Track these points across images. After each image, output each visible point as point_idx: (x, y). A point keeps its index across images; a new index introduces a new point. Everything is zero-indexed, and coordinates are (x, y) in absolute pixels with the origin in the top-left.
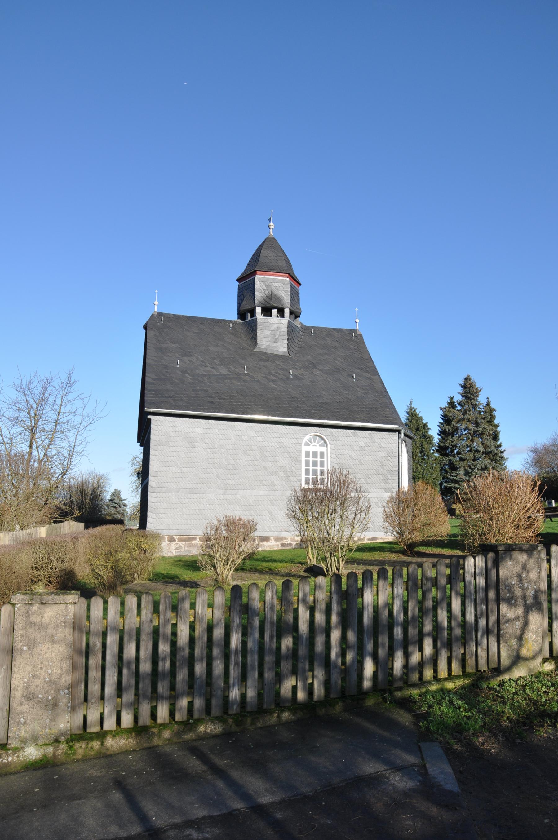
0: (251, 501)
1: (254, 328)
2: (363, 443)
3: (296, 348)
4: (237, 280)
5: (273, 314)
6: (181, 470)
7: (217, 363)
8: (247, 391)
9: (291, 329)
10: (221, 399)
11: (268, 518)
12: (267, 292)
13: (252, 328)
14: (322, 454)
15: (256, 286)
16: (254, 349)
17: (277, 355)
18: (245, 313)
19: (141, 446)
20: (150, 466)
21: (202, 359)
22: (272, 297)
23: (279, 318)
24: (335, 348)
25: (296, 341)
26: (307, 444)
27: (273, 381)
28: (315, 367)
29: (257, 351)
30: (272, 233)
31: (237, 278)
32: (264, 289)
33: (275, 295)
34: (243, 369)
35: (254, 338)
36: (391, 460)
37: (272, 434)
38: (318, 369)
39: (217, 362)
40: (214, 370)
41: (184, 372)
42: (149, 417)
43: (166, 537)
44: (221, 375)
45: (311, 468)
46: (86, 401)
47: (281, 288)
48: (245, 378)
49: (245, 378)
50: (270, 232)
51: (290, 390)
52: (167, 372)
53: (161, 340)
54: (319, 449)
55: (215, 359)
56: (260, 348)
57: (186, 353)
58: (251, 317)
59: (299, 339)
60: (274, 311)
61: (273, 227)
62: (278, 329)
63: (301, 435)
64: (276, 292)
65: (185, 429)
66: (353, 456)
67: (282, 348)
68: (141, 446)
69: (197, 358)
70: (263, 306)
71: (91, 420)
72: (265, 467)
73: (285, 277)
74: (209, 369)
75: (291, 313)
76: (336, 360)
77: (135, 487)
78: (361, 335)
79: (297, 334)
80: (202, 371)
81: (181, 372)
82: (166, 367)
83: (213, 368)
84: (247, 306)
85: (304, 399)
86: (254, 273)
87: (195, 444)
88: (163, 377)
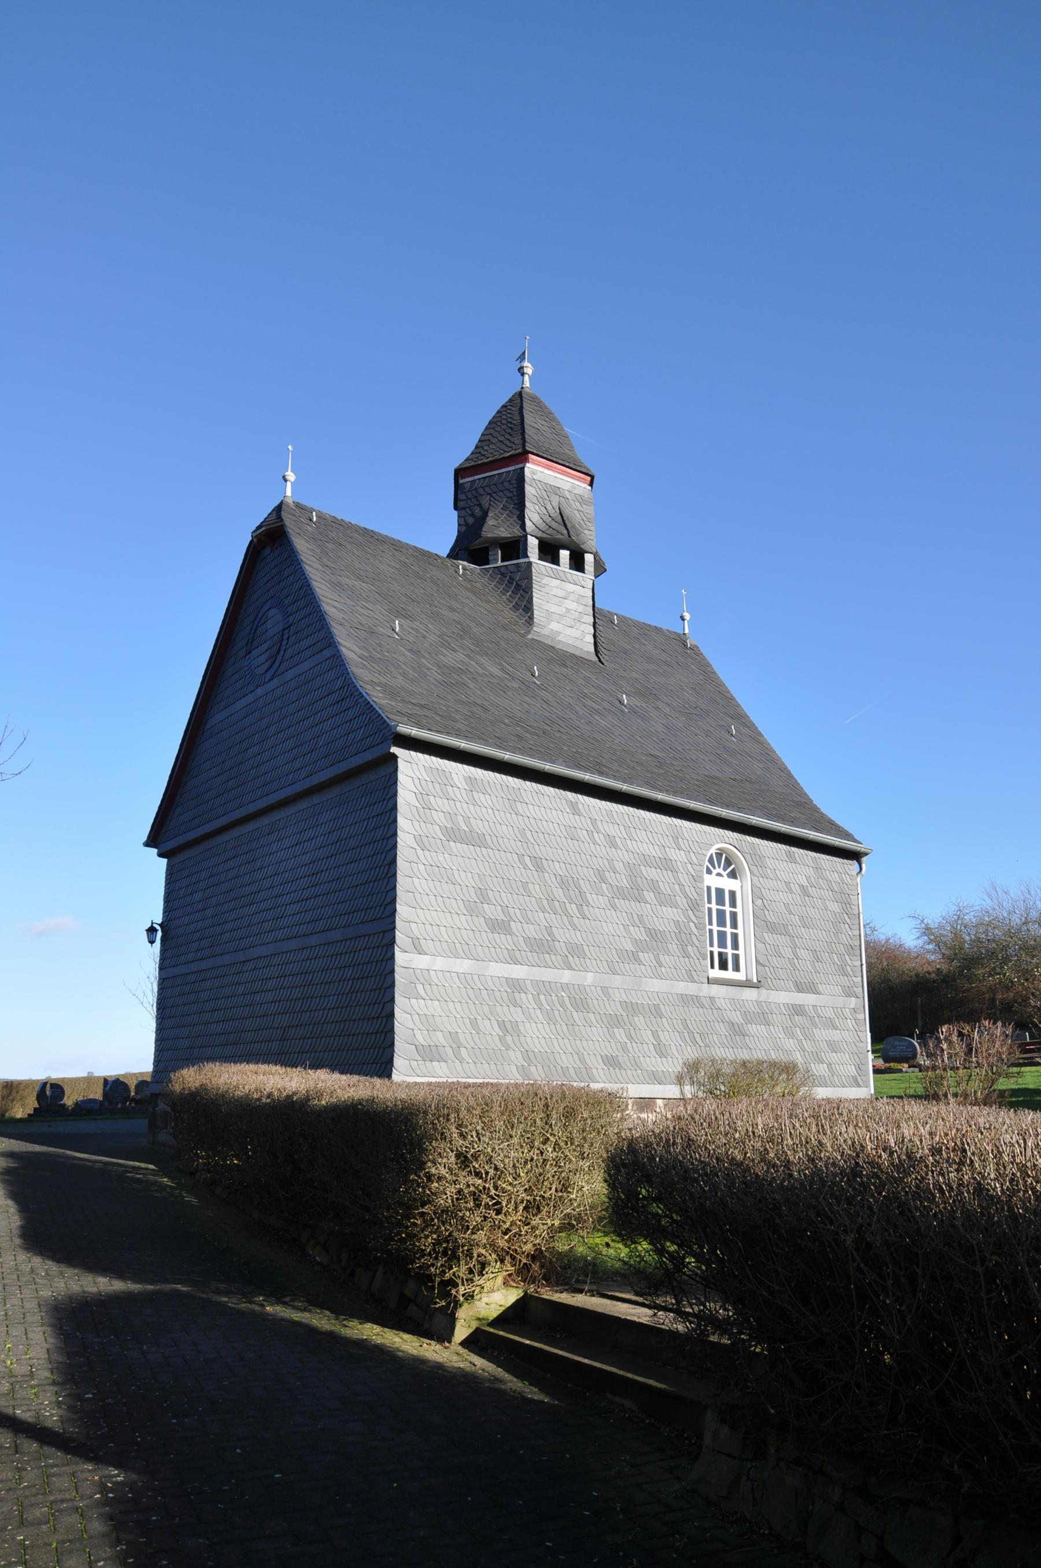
1: (524, 583)
5: (561, 561)
13: (519, 590)
14: (733, 894)
16: (529, 632)
19: (160, 855)
31: (456, 465)
35: (525, 607)
36: (848, 921)
42: (394, 750)
43: (630, 1102)
54: (728, 884)
60: (564, 554)
70: (545, 535)
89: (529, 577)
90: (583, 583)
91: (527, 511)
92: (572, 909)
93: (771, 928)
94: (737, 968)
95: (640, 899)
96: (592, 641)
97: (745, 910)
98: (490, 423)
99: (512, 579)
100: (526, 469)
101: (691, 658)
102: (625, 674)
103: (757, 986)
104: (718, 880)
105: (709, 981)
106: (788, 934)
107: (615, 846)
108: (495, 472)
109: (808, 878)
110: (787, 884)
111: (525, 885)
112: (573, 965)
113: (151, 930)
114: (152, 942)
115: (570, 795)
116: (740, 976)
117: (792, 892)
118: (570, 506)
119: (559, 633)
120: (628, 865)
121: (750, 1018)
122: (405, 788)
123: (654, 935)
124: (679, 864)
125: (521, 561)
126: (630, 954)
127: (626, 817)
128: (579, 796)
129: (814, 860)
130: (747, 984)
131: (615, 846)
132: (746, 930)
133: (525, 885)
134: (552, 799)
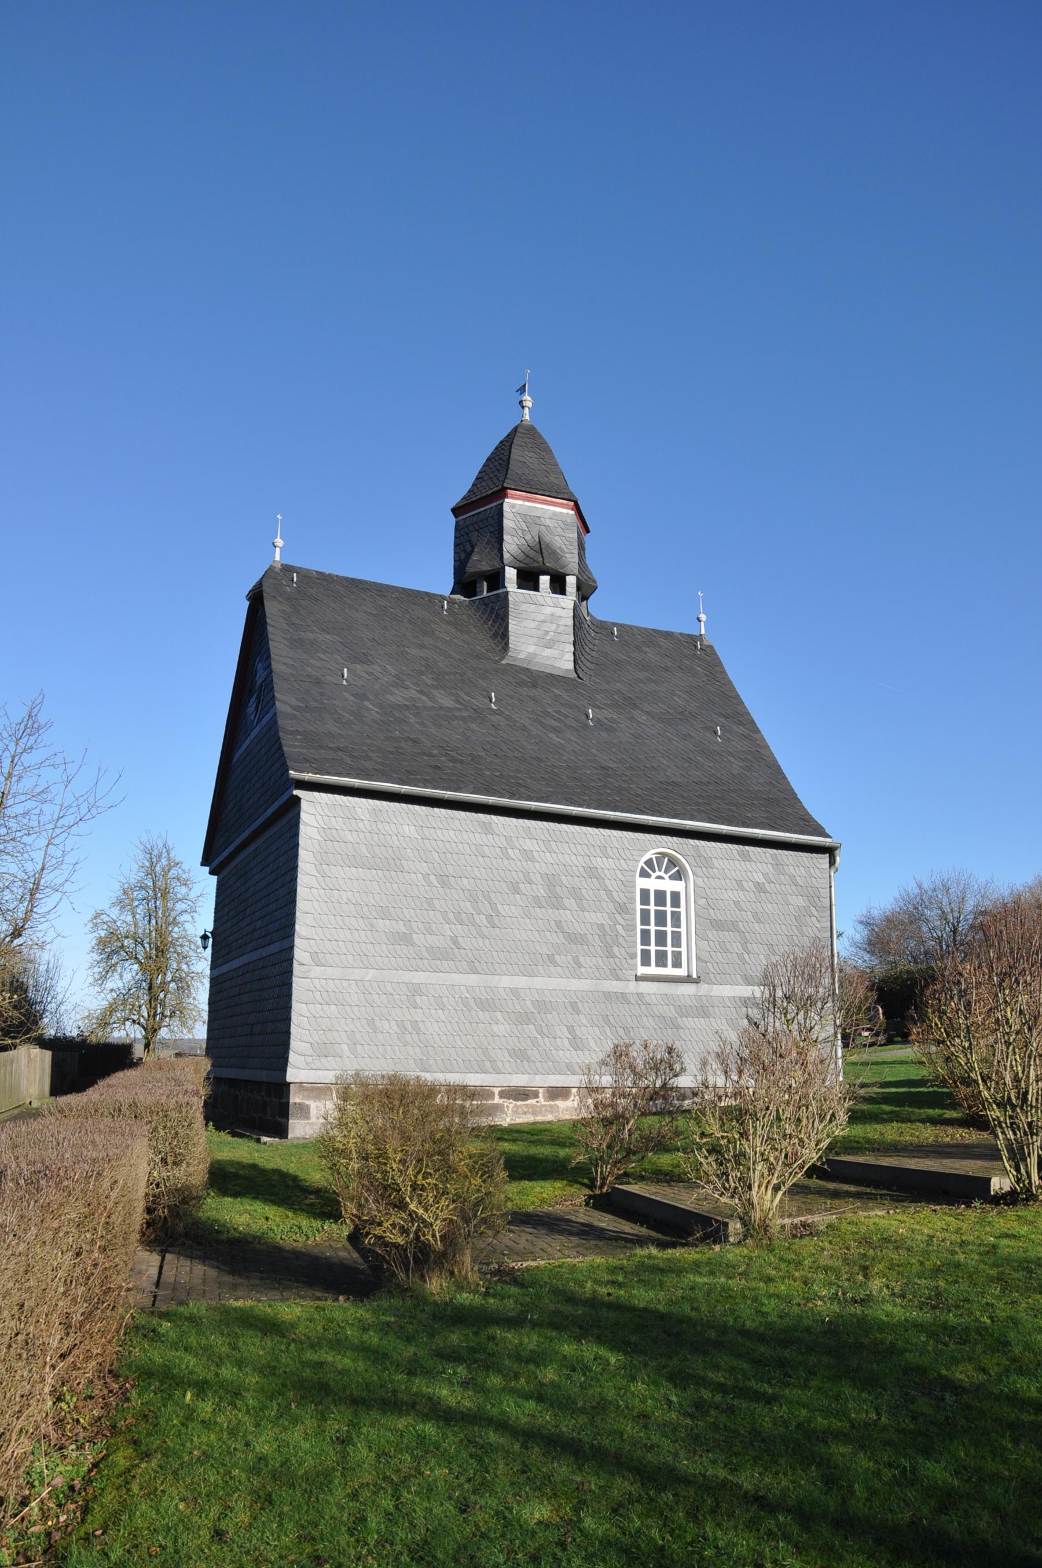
0: (528, 1003)
1: (501, 612)
2: (760, 875)
3: (588, 664)
5: (541, 586)
6: (372, 925)
7: (430, 682)
8: (504, 748)
10: (454, 761)
11: (566, 1043)
13: (497, 616)
14: (676, 896)
15: (506, 522)
16: (503, 658)
19: (211, 873)
20: (298, 914)
21: (394, 672)
22: (540, 547)
24: (666, 669)
25: (587, 649)
26: (644, 874)
27: (555, 730)
28: (635, 707)
31: (453, 505)
33: (548, 545)
34: (487, 701)
35: (502, 635)
36: (815, 913)
37: (572, 846)
38: (642, 711)
39: (427, 679)
40: (424, 698)
41: (362, 697)
42: (296, 792)
43: (541, 1090)
44: (441, 708)
45: (653, 928)
46: (71, 769)
48: (495, 719)
49: (495, 719)
51: (593, 751)
52: (322, 694)
53: (299, 622)
54: (670, 886)
55: (422, 673)
56: (515, 659)
57: (357, 658)
59: (591, 646)
60: (545, 580)
63: (634, 853)
64: (547, 538)
65: (380, 826)
66: (742, 904)
67: (561, 658)
68: (211, 873)
69: (384, 669)
70: (522, 565)
71: (84, 809)
72: (558, 923)
74: (412, 693)
76: (675, 694)
77: (97, 976)
78: (711, 647)
80: (398, 697)
81: (353, 695)
82: (318, 682)
83: (421, 692)
84: (480, 562)
85: (628, 773)
86: (501, 494)
87: (404, 863)
88: (315, 704)
89: (506, 606)
90: (563, 605)
91: (505, 544)
92: (481, 920)
93: (718, 925)
94: (677, 964)
95: (559, 906)
96: (572, 658)
97: (687, 910)
98: (488, 460)
99: (493, 609)
100: (505, 506)
101: (699, 659)
102: (607, 687)
103: (697, 981)
104: (661, 883)
105: (638, 979)
106: (737, 930)
107: (532, 860)
108: (482, 509)
109: (765, 876)
110: (739, 883)
111: (430, 901)
112: (480, 970)
113: (205, 937)
114: (205, 948)
115: (481, 816)
116: (682, 972)
117: (743, 889)
118: (551, 533)
119: (535, 655)
120: (546, 877)
121: (684, 1011)
122: (307, 825)
123: (574, 938)
124: (606, 871)
125: (500, 591)
126: (545, 957)
127: (546, 832)
128: (493, 817)
129: (773, 857)
130: (688, 979)
131: (532, 860)
132: (688, 928)
133: (430, 901)
134: (463, 822)
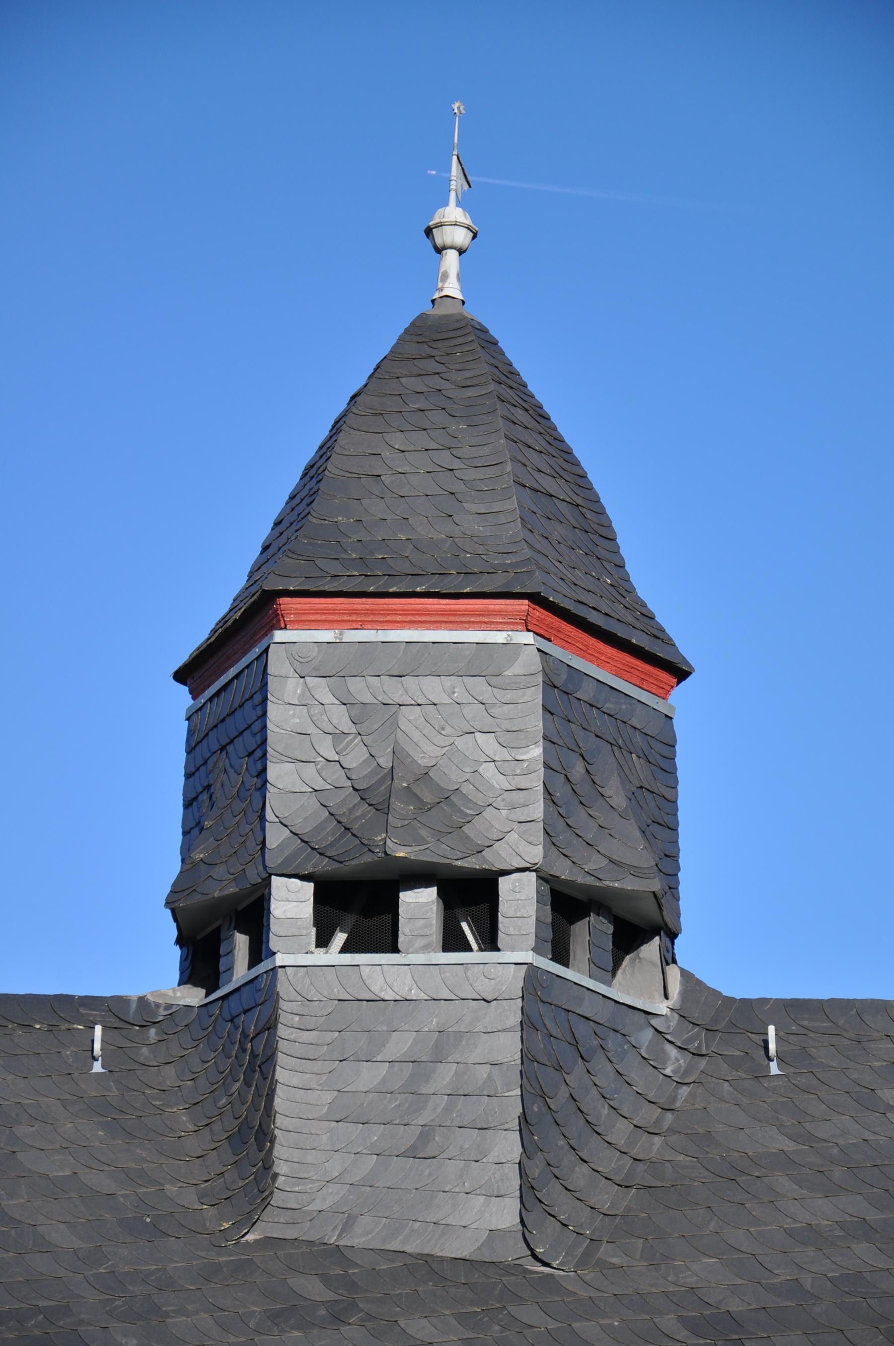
4: (181, 676)
9: (559, 1036)
12: (355, 758)
17: (428, 1266)
18: (216, 924)
23: (475, 956)
25: (620, 1131)
29: (267, 1242)
30: (452, 288)
32: (338, 736)
47: (473, 711)
50: (437, 276)
58: (344, 950)
60: (420, 905)
61: (461, 237)
62: (445, 1043)
67: (477, 1208)
70: (322, 865)
73: (508, 625)
75: (566, 905)
79: (638, 1075)
